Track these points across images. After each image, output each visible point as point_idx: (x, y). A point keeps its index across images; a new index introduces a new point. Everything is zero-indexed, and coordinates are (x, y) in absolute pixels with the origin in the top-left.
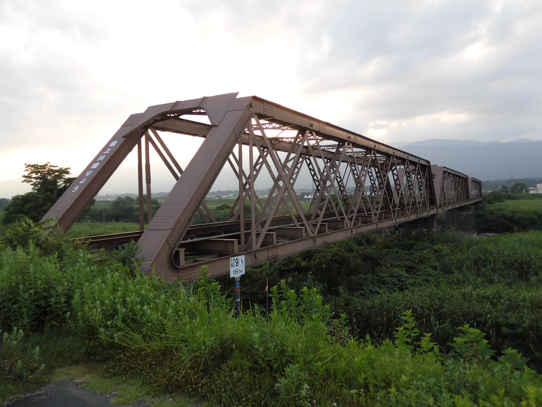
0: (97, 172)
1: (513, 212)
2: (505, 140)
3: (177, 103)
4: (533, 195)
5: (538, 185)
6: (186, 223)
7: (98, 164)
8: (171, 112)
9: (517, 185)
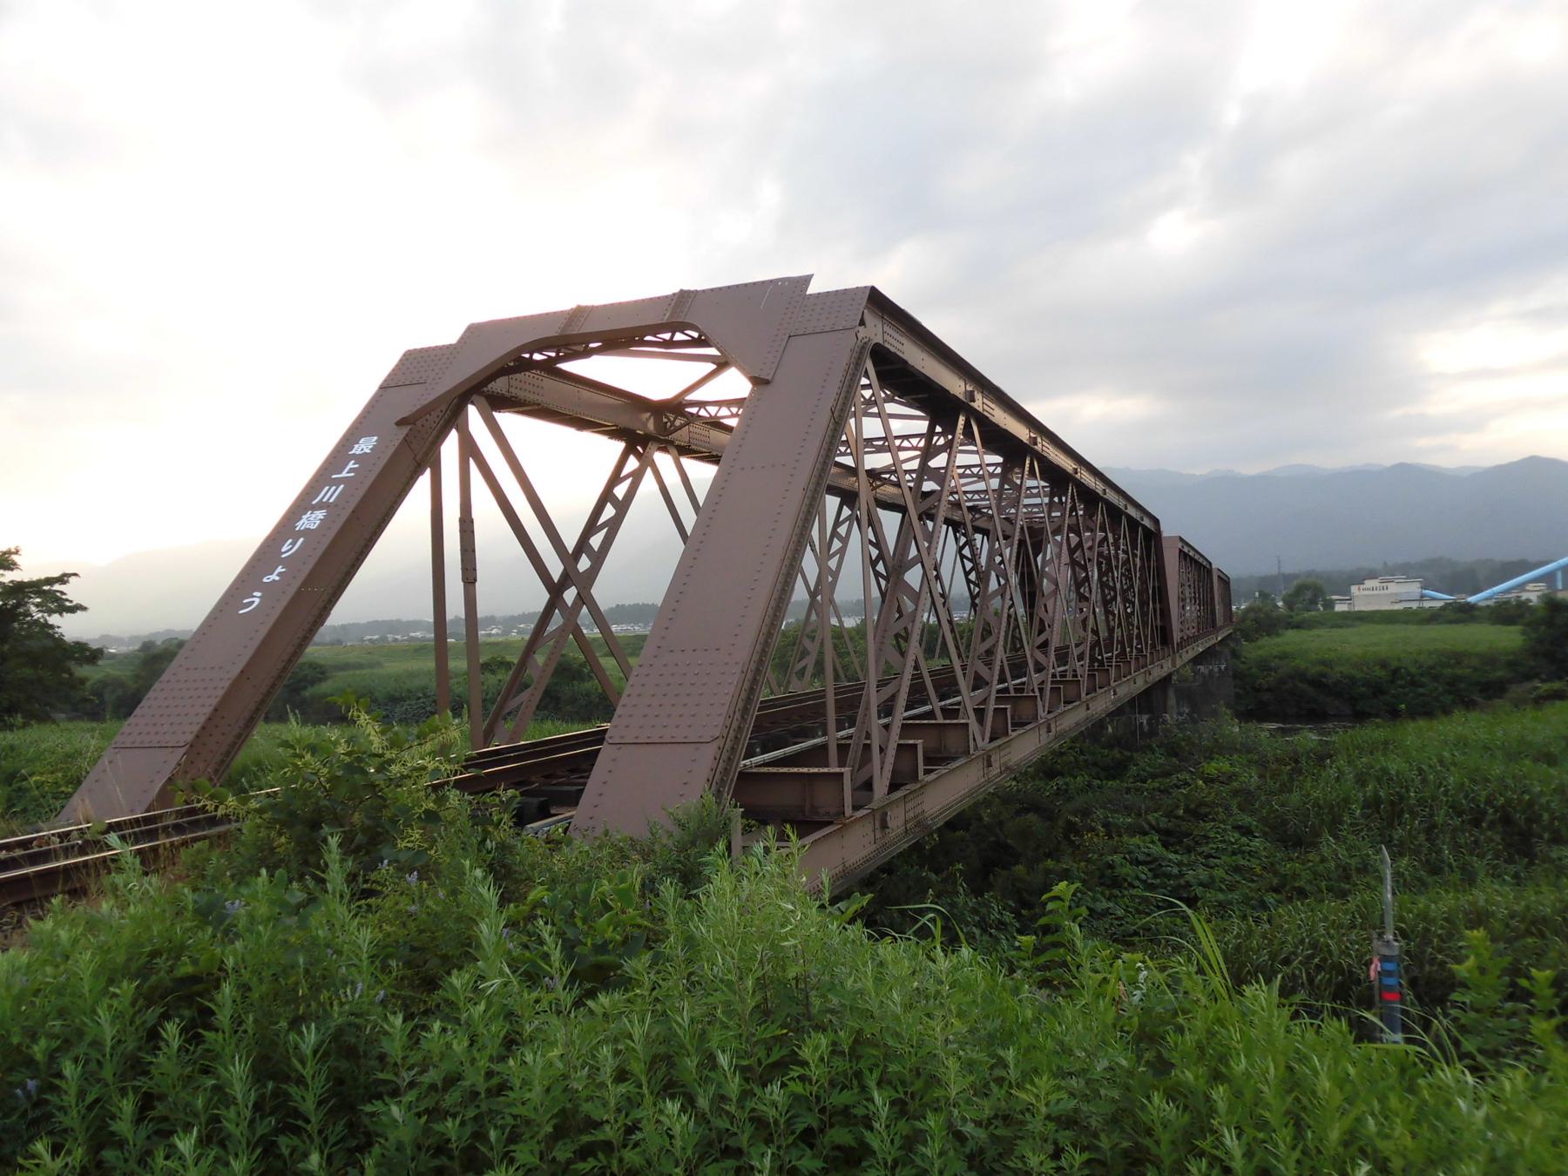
0: (326, 542)
1: (1323, 663)
2: (1250, 469)
3: (580, 313)
4: (1344, 615)
5: (1354, 589)
6: (738, 715)
7: (320, 514)
8: (540, 346)
9: (1301, 589)
